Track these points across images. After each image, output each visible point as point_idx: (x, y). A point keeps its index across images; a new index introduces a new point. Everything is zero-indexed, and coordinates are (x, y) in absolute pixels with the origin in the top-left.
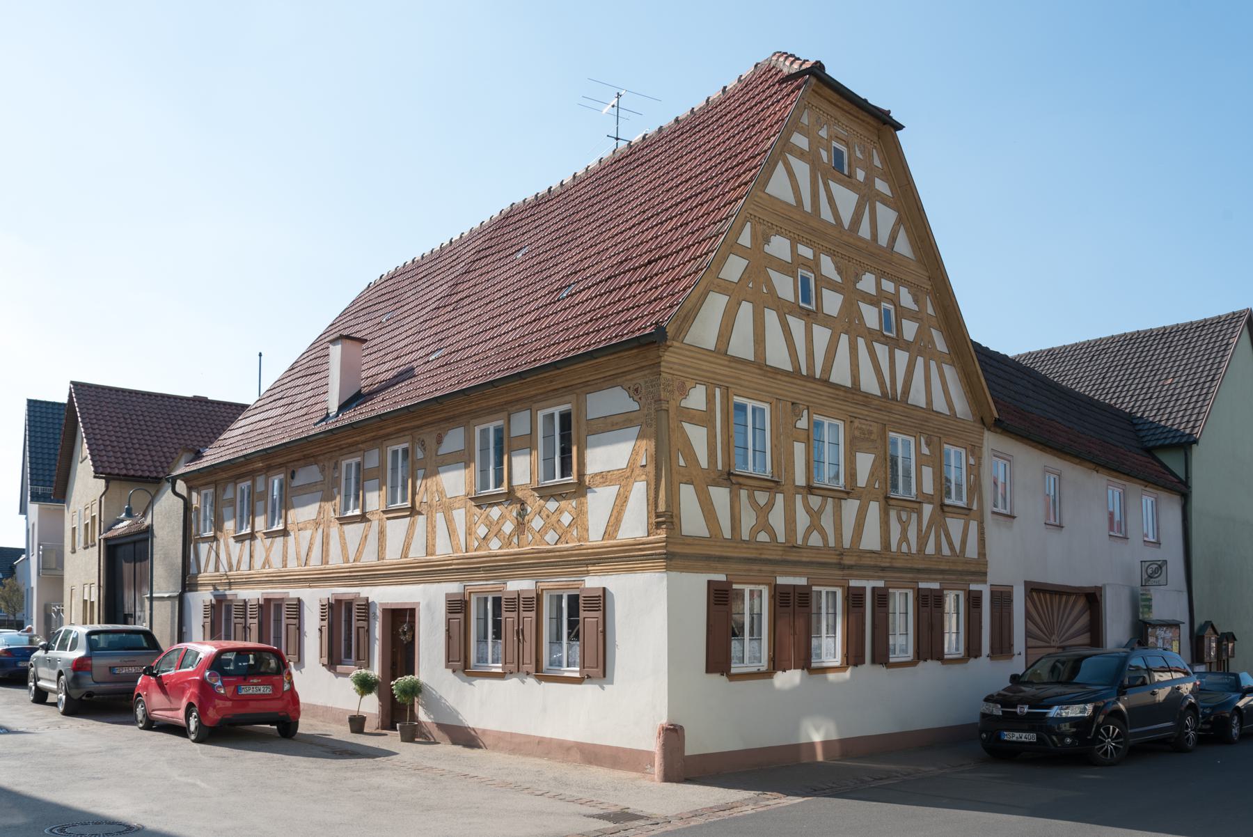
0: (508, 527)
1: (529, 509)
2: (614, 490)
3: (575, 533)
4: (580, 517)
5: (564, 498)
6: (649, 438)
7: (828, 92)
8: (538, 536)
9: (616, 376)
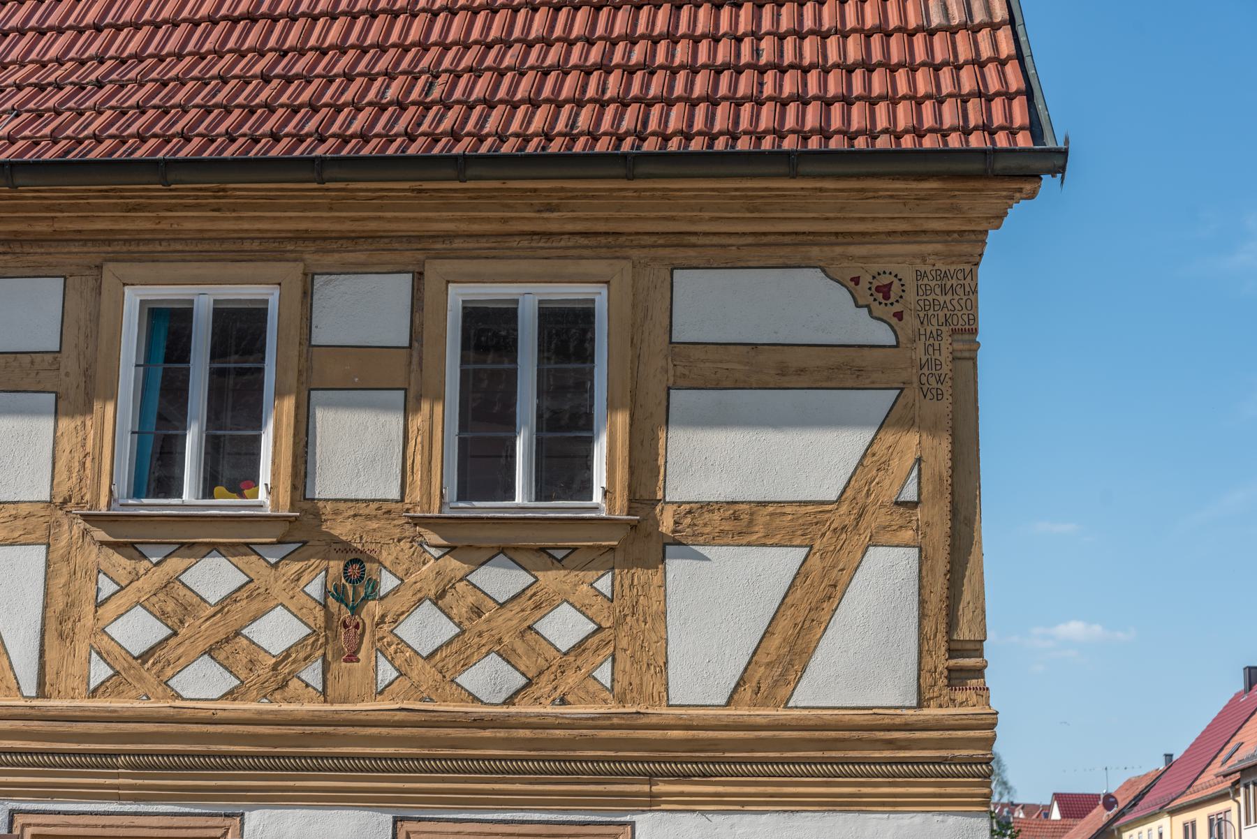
0: (277, 631)
1: (388, 582)
2: (786, 561)
3: (604, 674)
4: (632, 633)
5: (559, 563)
6: (932, 429)
7: (1022, 39)
8: (424, 674)
9: (813, 238)
